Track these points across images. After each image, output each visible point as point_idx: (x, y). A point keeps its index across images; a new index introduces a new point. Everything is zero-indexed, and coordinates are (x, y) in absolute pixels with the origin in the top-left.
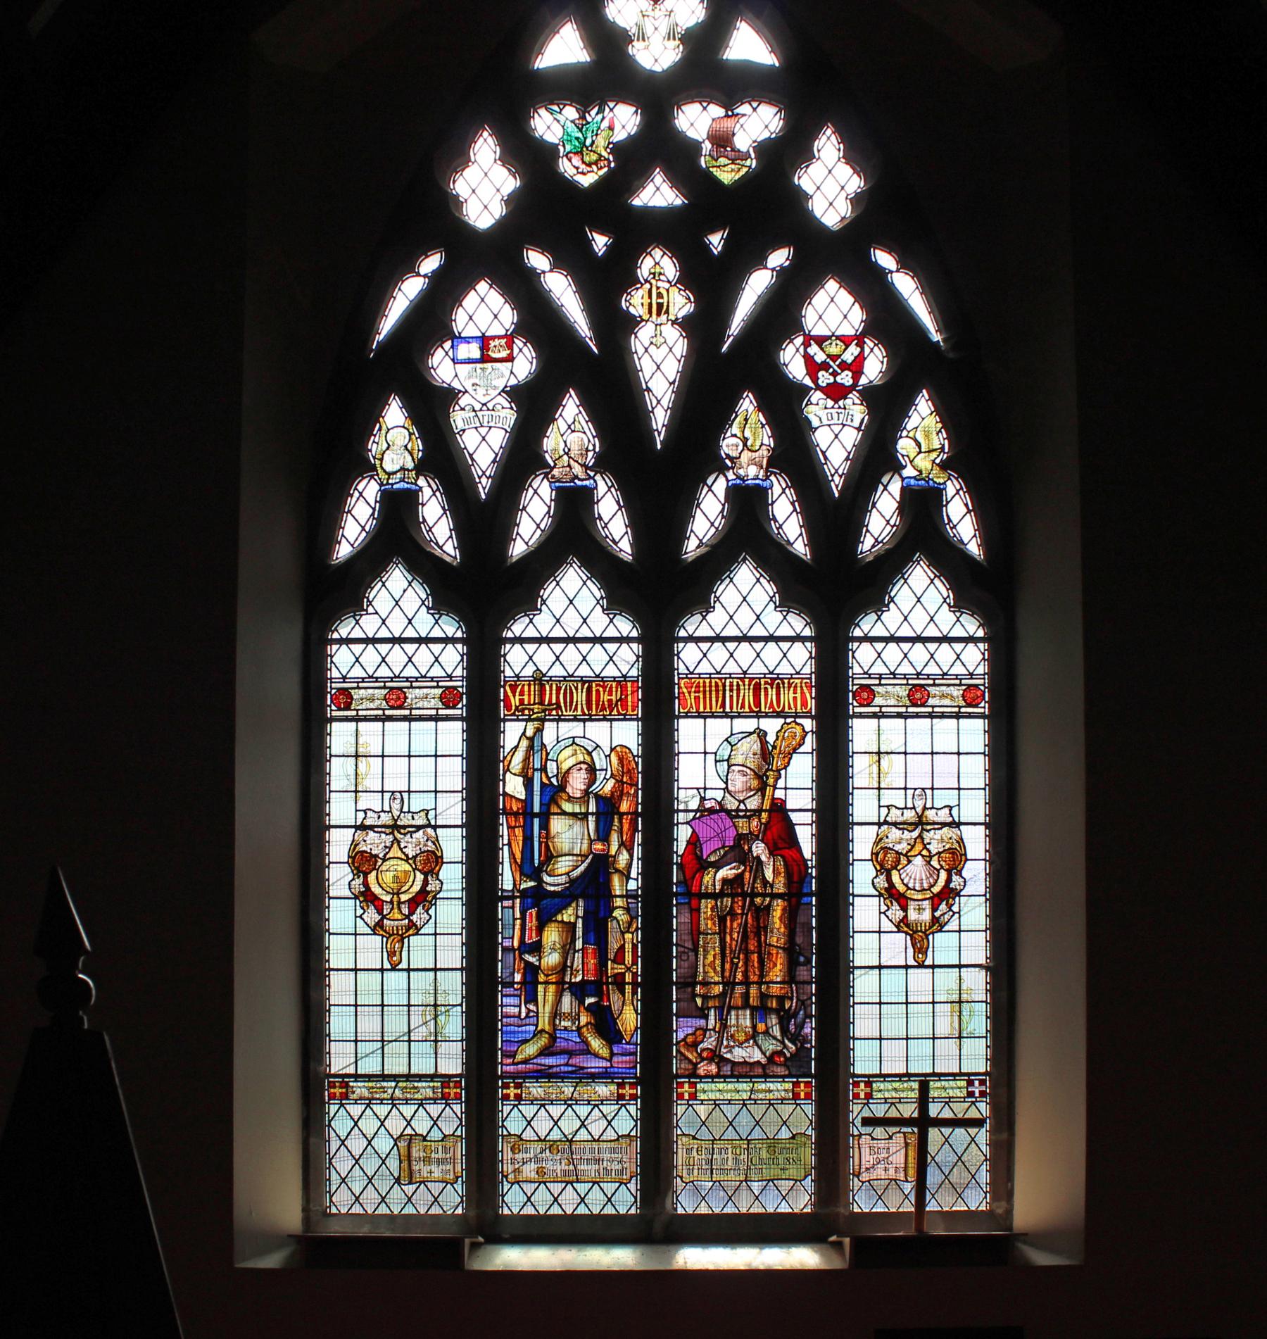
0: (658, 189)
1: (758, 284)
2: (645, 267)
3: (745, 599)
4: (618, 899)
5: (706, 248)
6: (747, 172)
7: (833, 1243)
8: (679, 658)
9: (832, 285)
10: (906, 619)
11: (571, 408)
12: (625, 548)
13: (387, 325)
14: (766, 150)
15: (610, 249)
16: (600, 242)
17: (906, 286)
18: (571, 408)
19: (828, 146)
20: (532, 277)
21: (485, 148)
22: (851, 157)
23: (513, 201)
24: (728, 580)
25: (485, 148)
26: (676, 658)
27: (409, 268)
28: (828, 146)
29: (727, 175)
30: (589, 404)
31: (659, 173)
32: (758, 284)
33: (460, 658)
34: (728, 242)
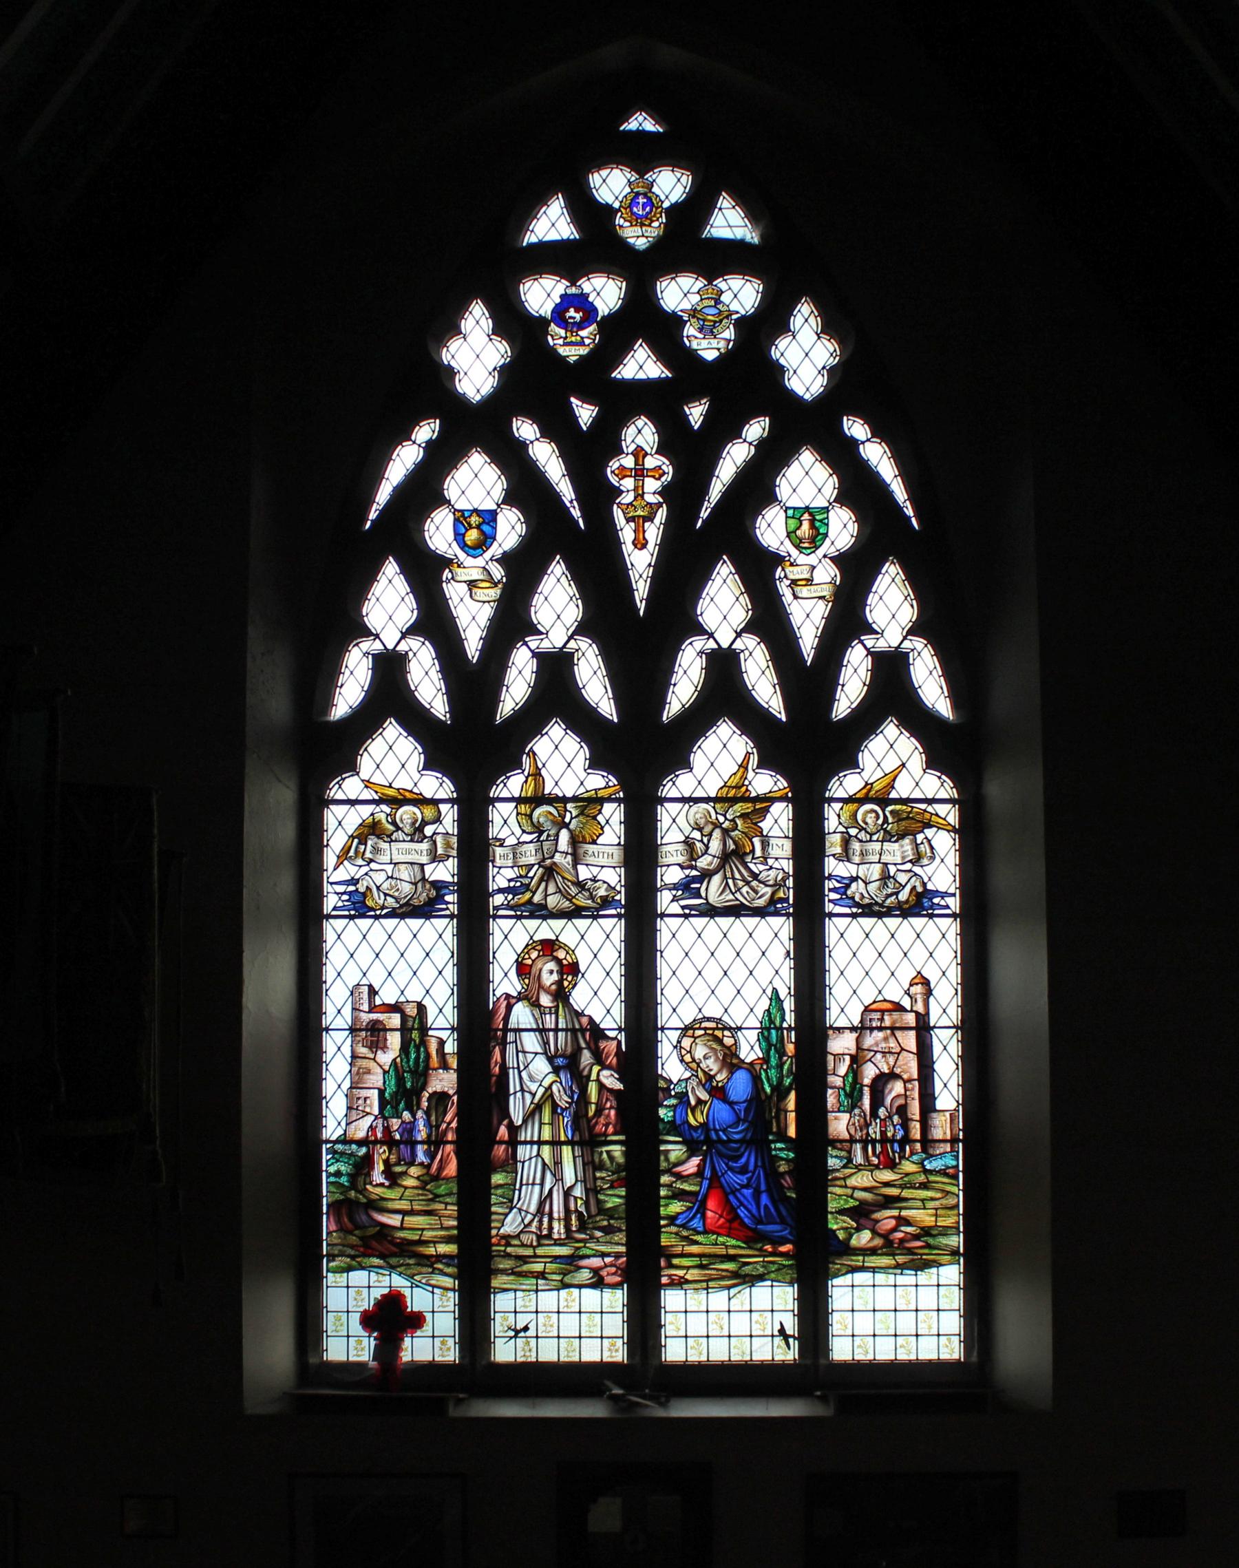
0: (639, 431)
1: (734, 457)
2: (629, 433)
3: (891, 746)
4: (599, 1181)
5: (685, 419)
6: (505, 1113)
7: (818, 1397)
8: (958, 1102)
9: (807, 457)
10: (391, 748)
11: (557, 572)
12: (607, 708)
13: (383, 494)
14: (744, 324)
15: (597, 422)
16: (585, 413)
17: (877, 455)
18: (557, 572)
19: (805, 318)
20: (521, 447)
21: (477, 319)
22: (829, 328)
23: (505, 372)
24: (502, 785)
25: (477, 319)
26: (960, 1102)
27: (404, 435)
28: (805, 318)
29: (709, 350)
30: (578, 575)
31: (641, 345)
32: (734, 457)
33: (330, 843)
34: (708, 417)
